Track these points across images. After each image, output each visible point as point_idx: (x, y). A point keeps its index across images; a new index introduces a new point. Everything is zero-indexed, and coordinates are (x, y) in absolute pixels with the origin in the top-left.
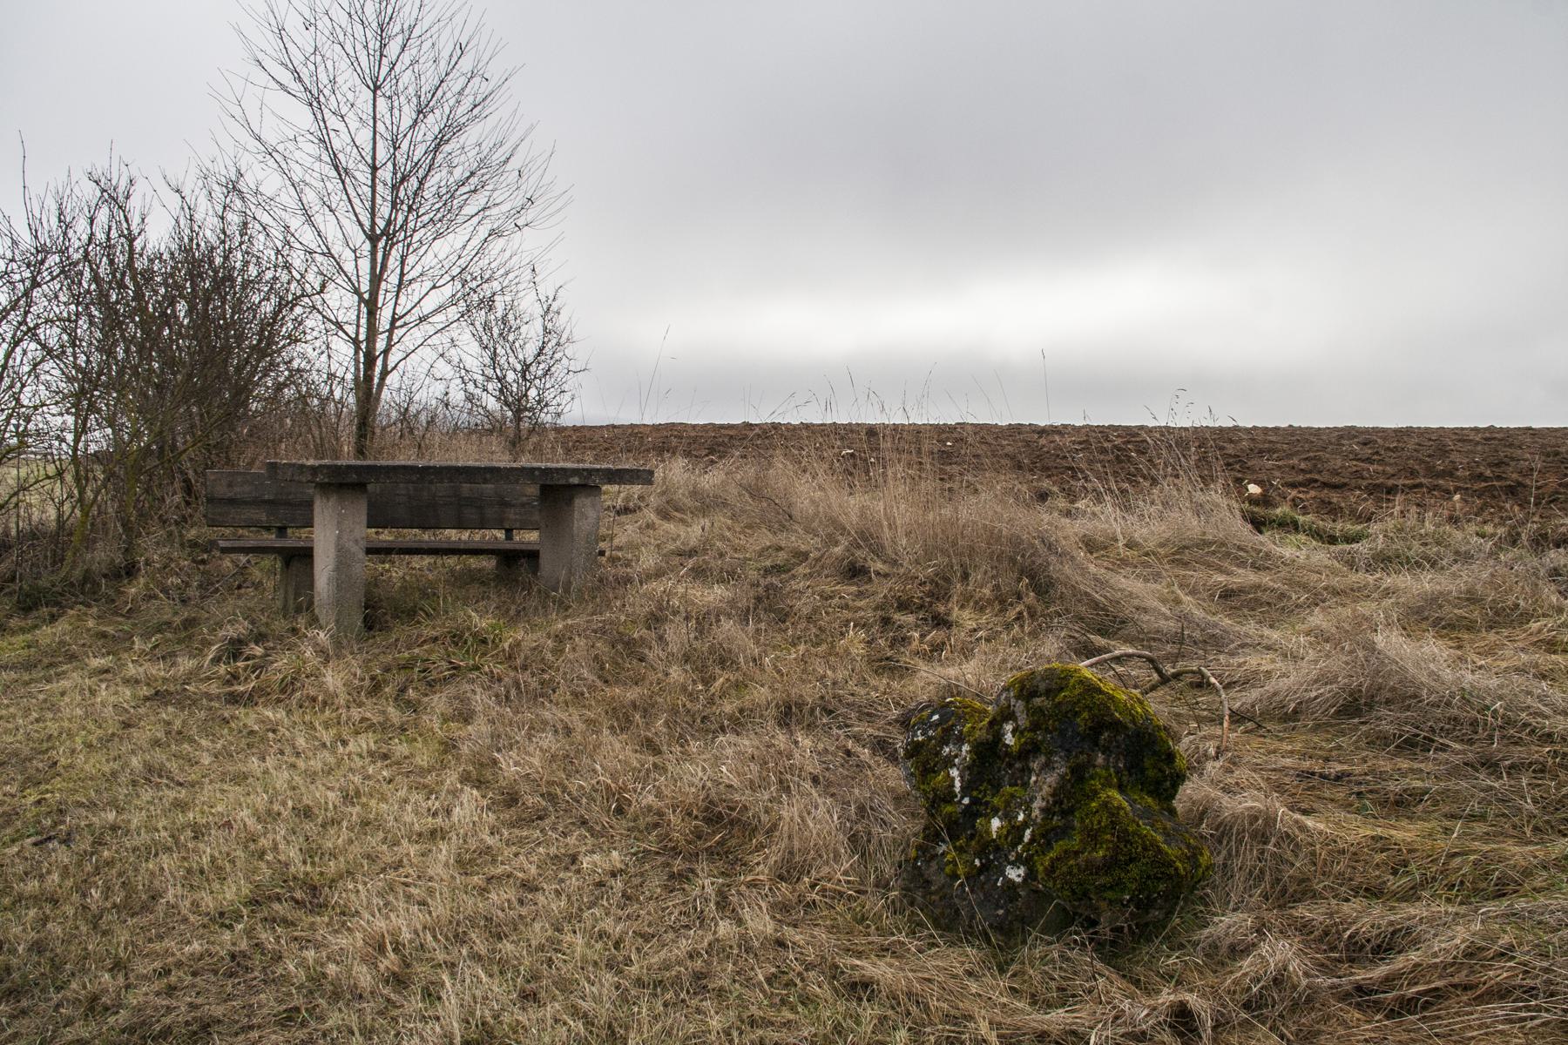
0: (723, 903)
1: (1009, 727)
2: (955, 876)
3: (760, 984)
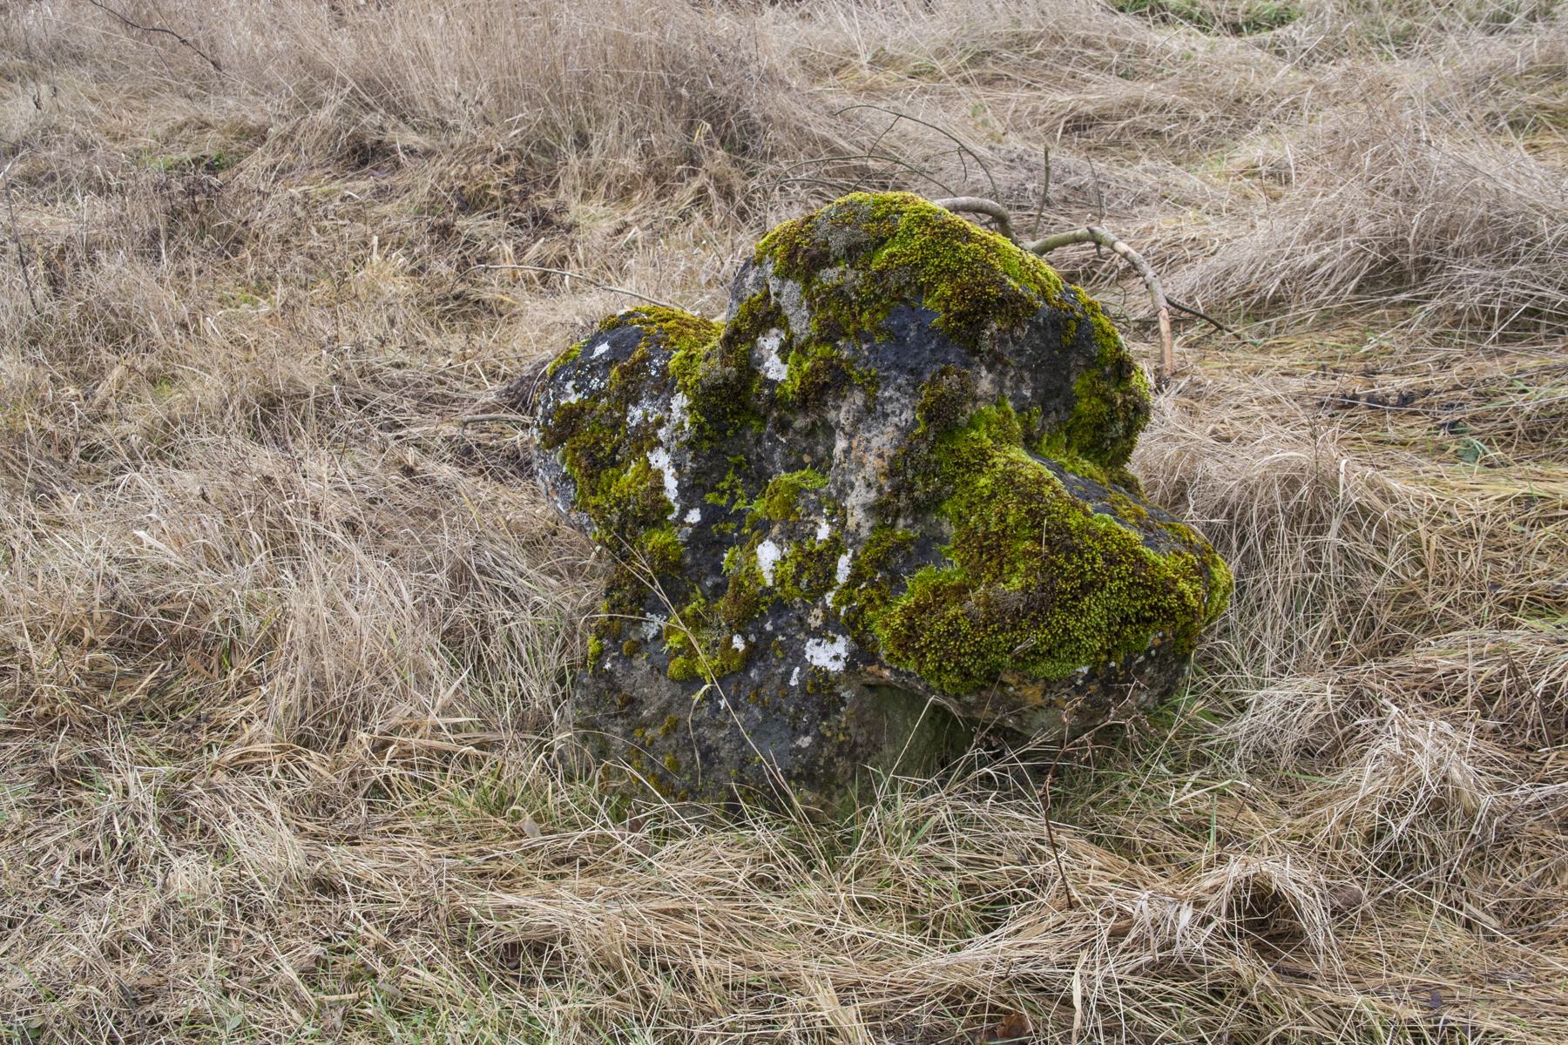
0: (176, 816)
1: (770, 343)
2: (693, 680)
3: (289, 988)
